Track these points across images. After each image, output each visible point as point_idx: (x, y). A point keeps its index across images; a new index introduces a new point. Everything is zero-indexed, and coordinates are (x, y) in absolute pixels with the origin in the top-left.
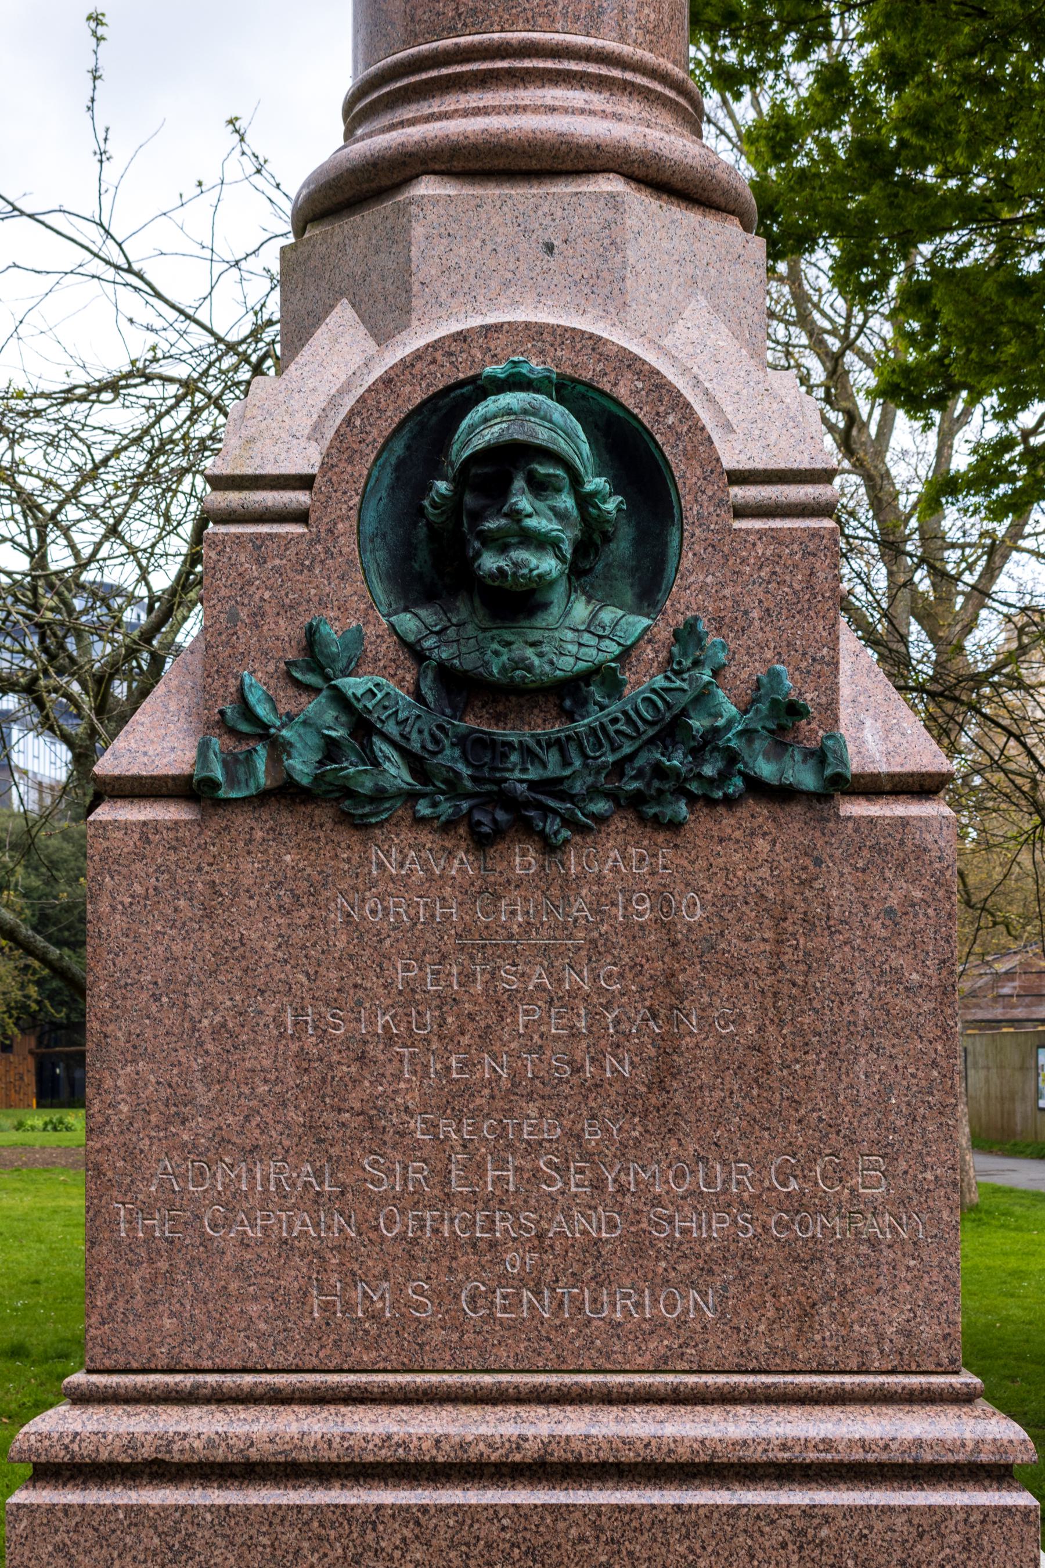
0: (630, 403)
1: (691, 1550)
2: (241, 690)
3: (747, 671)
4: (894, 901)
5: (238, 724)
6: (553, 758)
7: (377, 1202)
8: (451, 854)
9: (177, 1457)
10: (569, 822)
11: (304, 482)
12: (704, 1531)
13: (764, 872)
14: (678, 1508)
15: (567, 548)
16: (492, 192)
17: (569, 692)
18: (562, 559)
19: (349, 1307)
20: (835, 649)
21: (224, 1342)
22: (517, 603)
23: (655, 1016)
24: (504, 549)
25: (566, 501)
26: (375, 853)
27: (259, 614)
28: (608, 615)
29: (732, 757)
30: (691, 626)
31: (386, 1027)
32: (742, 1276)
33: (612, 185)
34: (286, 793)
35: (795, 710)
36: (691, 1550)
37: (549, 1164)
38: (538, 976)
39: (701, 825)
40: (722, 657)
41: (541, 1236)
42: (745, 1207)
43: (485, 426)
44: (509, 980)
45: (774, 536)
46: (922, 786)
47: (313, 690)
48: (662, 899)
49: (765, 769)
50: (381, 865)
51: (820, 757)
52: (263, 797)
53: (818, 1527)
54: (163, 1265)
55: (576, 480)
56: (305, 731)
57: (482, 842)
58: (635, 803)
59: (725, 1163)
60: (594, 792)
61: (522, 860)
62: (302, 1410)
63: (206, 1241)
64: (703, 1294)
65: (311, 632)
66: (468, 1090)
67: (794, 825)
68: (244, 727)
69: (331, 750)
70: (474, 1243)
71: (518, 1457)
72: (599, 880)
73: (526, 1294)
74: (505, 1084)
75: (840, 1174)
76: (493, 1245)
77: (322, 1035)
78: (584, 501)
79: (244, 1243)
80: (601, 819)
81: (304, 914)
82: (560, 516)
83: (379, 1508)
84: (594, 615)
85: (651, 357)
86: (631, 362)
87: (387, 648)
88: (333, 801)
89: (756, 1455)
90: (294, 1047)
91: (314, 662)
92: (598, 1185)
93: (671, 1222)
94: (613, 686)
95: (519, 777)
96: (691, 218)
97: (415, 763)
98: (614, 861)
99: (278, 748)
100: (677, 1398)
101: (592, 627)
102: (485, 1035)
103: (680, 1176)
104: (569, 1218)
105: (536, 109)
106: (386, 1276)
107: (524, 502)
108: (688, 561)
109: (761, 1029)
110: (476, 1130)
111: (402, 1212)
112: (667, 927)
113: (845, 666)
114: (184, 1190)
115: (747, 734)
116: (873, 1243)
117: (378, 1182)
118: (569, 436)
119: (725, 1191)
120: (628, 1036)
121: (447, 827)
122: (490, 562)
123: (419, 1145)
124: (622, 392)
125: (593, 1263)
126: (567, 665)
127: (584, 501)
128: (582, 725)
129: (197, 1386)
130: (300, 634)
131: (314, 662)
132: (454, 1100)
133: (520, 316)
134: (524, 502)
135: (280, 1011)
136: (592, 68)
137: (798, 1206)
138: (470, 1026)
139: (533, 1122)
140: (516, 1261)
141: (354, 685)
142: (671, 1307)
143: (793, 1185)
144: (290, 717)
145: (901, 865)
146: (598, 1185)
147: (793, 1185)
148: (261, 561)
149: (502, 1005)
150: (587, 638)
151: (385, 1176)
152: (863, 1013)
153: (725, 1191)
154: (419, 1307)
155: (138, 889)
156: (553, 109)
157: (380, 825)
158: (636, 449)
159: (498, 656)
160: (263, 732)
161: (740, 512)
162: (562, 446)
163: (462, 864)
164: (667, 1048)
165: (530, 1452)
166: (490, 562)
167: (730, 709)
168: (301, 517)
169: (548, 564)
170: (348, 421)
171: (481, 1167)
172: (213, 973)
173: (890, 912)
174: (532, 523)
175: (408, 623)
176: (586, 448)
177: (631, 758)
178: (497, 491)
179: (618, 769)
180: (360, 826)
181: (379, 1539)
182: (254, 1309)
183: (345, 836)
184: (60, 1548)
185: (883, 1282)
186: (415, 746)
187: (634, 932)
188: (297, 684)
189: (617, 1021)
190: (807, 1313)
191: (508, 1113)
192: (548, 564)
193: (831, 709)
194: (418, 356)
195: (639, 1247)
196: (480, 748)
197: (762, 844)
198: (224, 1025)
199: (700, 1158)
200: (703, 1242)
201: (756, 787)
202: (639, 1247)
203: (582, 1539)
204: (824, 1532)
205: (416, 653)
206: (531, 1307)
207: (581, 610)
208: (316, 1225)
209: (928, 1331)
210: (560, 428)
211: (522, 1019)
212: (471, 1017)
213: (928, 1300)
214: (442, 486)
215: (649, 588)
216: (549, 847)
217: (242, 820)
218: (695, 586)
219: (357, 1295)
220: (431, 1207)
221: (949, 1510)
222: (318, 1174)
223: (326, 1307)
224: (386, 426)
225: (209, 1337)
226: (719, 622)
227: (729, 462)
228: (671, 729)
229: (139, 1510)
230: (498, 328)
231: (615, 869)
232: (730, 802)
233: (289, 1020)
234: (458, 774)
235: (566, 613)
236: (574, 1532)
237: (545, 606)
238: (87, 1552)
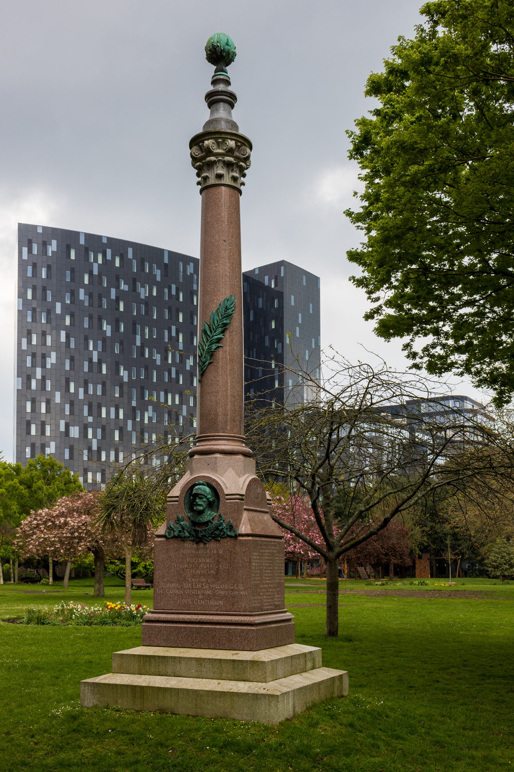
3: (227, 521)
7: (185, 589)
11: (178, 497)
17: (207, 523)
33: (218, 455)
34: (174, 537)
39: (222, 541)
44: (200, 561)
49: (229, 533)
52: (172, 538)
56: (177, 529)
57: (197, 543)
58: (214, 538)
60: (209, 536)
61: (202, 545)
66: (195, 575)
67: (233, 541)
69: (180, 531)
75: (237, 586)
82: (204, 502)
86: (214, 480)
87: (187, 518)
89: (223, 622)
91: (178, 520)
94: (212, 523)
95: (200, 535)
97: (189, 533)
98: (212, 545)
99: (174, 531)
100: (236, 615)
102: (197, 568)
107: (197, 501)
115: (227, 529)
121: (193, 541)
125: (209, 597)
126: (205, 520)
131: (178, 520)
132: (194, 576)
133: (206, 475)
137: (233, 590)
139: (203, 579)
140: (201, 597)
141: (182, 523)
149: (199, 564)
151: (186, 585)
160: (172, 529)
161: (227, 499)
164: (218, 569)
165: (198, 620)
168: (177, 501)
175: (189, 515)
179: (212, 534)
180: (183, 541)
183: (182, 542)
187: (214, 554)
190: (233, 604)
195: (214, 595)
196: (196, 531)
201: (228, 536)
202: (214, 595)
205: (189, 518)
209: (247, 607)
216: (205, 544)
217: (171, 540)
224: (187, 489)
226: (224, 514)
232: (225, 538)
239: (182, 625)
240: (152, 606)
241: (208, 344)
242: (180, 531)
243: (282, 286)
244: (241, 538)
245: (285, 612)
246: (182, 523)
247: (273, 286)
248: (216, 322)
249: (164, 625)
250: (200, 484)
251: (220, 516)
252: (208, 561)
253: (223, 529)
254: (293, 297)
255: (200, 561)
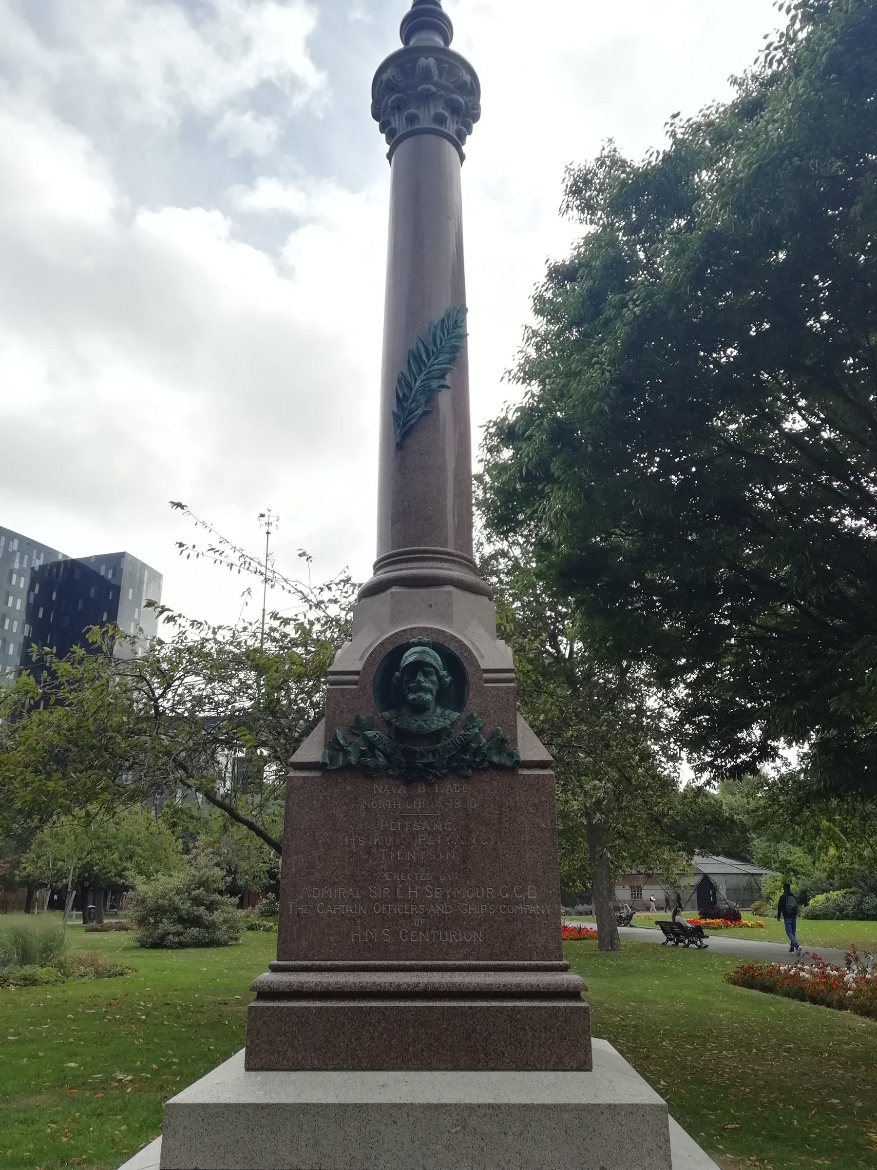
0: (453, 650)
1: (474, 1023)
2: (336, 735)
3: (489, 729)
4: (536, 801)
5: (332, 745)
6: (430, 756)
8: (398, 787)
9: (305, 990)
10: (436, 776)
11: (357, 673)
12: (478, 1016)
13: (496, 792)
14: (470, 1007)
15: (434, 692)
16: (414, 590)
17: (437, 735)
18: (432, 694)
19: (363, 937)
20: (516, 722)
21: (322, 950)
22: (420, 708)
23: (462, 839)
24: (415, 693)
25: (435, 678)
26: (375, 786)
27: (342, 712)
28: (447, 712)
29: (485, 755)
30: (472, 715)
31: (377, 842)
32: (491, 926)
33: (450, 588)
34: (348, 767)
35: (504, 741)
36: (474, 1023)
37: (429, 888)
38: (425, 825)
40: (482, 724)
41: (426, 913)
42: (492, 903)
43: (410, 657)
44: (416, 827)
45: (496, 688)
46: (543, 765)
47: (357, 735)
48: (464, 800)
49: (495, 759)
50: (377, 790)
51: (511, 755)
52: (340, 770)
53: (516, 1014)
54: (303, 923)
55: (437, 672)
59: (485, 888)
61: (421, 789)
62: (347, 974)
63: (317, 915)
64: (479, 933)
65: (357, 718)
68: (337, 747)
69: (362, 754)
70: (404, 915)
71: (417, 989)
72: (445, 793)
73: (421, 933)
74: (415, 861)
75: (521, 891)
76: (410, 916)
77: (357, 845)
78: (440, 678)
79: (330, 915)
80: (445, 775)
81: (353, 806)
82: (432, 682)
83: (371, 1007)
84: (443, 712)
85: (459, 637)
88: (363, 771)
90: (348, 849)
91: (357, 727)
92: (444, 895)
93: (468, 908)
94: (449, 735)
95: (420, 762)
96: (473, 597)
98: (450, 788)
99: (346, 753)
101: (442, 715)
103: (471, 892)
104: (435, 907)
105: (427, 568)
106: (375, 927)
107: (422, 679)
108: (471, 696)
109: (496, 843)
110: (406, 877)
111: (381, 905)
112: (466, 810)
113: (519, 729)
114: (311, 897)
115: (489, 749)
116: (533, 915)
117: (374, 895)
118: (435, 659)
119: (485, 897)
120: (454, 845)
122: (411, 697)
123: (387, 882)
124: (451, 647)
126: (434, 727)
127: (440, 678)
128: (438, 746)
129: (313, 965)
130: (354, 718)
133: (422, 625)
134: (422, 679)
135: (344, 837)
136: (444, 557)
137: (508, 902)
138: (404, 842)
140: (418, 922)
141: (370, 733)
142: (468, 938)
143: (507, 896)
144: (350, 743)
145: (538, 790)
146: (444, 895)
147: (507, 896)
148: (343, 696)
150: (441, 719)
152: (528, 838)
153: (485, 897)
154: (386, 938)
155: (301, 798)
156: (432, 568)
157: (377, 777)
158: (456, 662)
159: (414, 723)
160: (342, 749)
161: (487, 681)
162: (434, 663)
163: (402, 790)
166: (411, 697)
167: (484, 741)
169: (429, 697)
170: (370, 655)
171: (407, 889)
172: (323, 825)
173: (535, 805)
174: (424, 684)
175: (386, 714)
176: (440, 663)
177: (454, 755)
178: (413, 675)
179: (450, 760)
181: (371, 1019)
182: (332, 938)
184: (265, 1023)
185: (536, 929)
186: (388, 751)
188: (353, 733)
189: (450, 840)
191: (416, 871)
192: (429, 697)
193: (515, 740)
194: (391, 636)
197: (495, 783)
198: (326, 842)
199: (477, 886)
200: (478, 915)
201: (492, 765)
203: (438, 1019)
204: (518, 1016)
205: (389, 723)
206: (423, 937)
207: (439, 711)
208: (353, 909)
210: (434, 658)
211: (420, 840)
212: (404, 839)
213: (551, 935)
214: (398, 674)
215: (459, 705)
216: (429, 784)
218: (473, 703)
219: (366, 934)
220: (391, 903)
221: (559, 1008)
222: (354, 892)
223: (356, 938)
224: (382, 657)
225: (317, 948)
226: (480, 714)
227: (482, 667)
228: (465, 746)
229: (292, 1008)
230: (415, 628)
231: (449, 791)
232: (485, 770)
233: (347, 840)
234: (401, 761)
235: (434, 711)
236: (435, 1016)
237: (428, 709)
238: (274, 1024)
239: (374, 1004)
240: (274, 951)
241: (422, 377)
242: (362, 754)
243: (121, 579)
244: (525, 772)
245: (565, 969)
246: (370, 733)
247: (110, 577)
248: (438, 342)
249: (318, 1004)
250: (419, 644)
251: (471, 718)
252: (437, 827)
253: (479, 748)
254: (131, 591)
255: (416, 827)
